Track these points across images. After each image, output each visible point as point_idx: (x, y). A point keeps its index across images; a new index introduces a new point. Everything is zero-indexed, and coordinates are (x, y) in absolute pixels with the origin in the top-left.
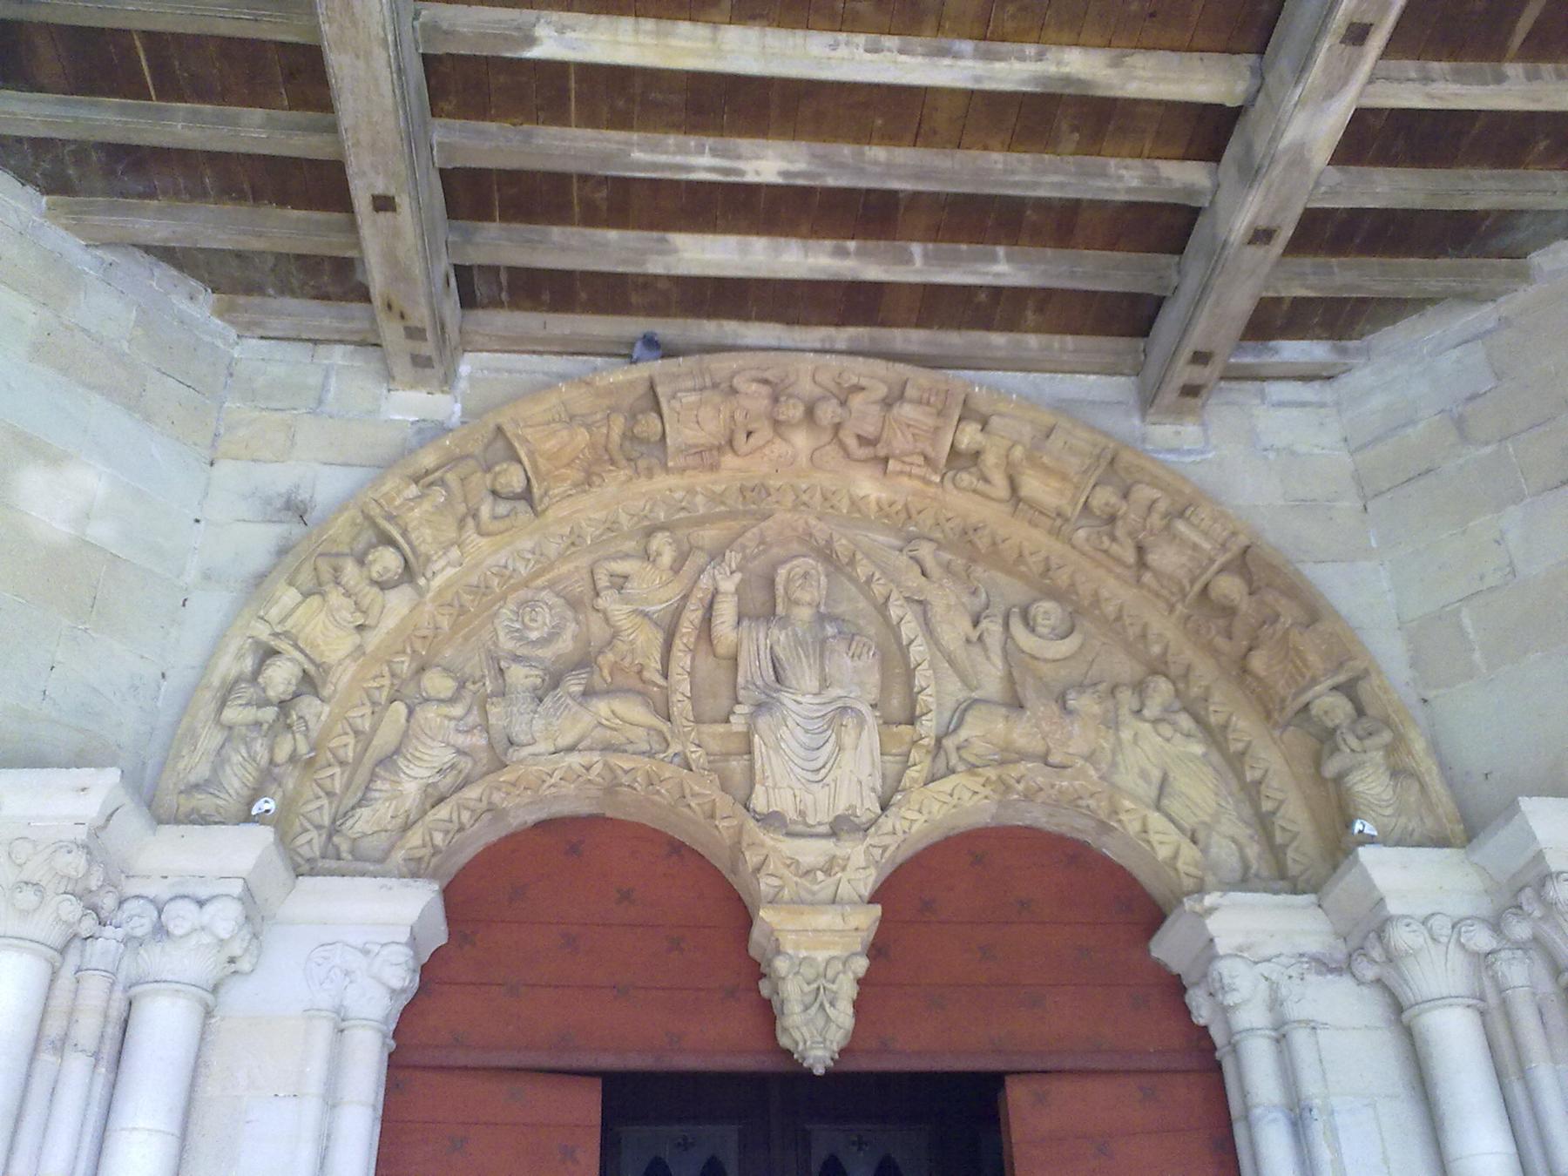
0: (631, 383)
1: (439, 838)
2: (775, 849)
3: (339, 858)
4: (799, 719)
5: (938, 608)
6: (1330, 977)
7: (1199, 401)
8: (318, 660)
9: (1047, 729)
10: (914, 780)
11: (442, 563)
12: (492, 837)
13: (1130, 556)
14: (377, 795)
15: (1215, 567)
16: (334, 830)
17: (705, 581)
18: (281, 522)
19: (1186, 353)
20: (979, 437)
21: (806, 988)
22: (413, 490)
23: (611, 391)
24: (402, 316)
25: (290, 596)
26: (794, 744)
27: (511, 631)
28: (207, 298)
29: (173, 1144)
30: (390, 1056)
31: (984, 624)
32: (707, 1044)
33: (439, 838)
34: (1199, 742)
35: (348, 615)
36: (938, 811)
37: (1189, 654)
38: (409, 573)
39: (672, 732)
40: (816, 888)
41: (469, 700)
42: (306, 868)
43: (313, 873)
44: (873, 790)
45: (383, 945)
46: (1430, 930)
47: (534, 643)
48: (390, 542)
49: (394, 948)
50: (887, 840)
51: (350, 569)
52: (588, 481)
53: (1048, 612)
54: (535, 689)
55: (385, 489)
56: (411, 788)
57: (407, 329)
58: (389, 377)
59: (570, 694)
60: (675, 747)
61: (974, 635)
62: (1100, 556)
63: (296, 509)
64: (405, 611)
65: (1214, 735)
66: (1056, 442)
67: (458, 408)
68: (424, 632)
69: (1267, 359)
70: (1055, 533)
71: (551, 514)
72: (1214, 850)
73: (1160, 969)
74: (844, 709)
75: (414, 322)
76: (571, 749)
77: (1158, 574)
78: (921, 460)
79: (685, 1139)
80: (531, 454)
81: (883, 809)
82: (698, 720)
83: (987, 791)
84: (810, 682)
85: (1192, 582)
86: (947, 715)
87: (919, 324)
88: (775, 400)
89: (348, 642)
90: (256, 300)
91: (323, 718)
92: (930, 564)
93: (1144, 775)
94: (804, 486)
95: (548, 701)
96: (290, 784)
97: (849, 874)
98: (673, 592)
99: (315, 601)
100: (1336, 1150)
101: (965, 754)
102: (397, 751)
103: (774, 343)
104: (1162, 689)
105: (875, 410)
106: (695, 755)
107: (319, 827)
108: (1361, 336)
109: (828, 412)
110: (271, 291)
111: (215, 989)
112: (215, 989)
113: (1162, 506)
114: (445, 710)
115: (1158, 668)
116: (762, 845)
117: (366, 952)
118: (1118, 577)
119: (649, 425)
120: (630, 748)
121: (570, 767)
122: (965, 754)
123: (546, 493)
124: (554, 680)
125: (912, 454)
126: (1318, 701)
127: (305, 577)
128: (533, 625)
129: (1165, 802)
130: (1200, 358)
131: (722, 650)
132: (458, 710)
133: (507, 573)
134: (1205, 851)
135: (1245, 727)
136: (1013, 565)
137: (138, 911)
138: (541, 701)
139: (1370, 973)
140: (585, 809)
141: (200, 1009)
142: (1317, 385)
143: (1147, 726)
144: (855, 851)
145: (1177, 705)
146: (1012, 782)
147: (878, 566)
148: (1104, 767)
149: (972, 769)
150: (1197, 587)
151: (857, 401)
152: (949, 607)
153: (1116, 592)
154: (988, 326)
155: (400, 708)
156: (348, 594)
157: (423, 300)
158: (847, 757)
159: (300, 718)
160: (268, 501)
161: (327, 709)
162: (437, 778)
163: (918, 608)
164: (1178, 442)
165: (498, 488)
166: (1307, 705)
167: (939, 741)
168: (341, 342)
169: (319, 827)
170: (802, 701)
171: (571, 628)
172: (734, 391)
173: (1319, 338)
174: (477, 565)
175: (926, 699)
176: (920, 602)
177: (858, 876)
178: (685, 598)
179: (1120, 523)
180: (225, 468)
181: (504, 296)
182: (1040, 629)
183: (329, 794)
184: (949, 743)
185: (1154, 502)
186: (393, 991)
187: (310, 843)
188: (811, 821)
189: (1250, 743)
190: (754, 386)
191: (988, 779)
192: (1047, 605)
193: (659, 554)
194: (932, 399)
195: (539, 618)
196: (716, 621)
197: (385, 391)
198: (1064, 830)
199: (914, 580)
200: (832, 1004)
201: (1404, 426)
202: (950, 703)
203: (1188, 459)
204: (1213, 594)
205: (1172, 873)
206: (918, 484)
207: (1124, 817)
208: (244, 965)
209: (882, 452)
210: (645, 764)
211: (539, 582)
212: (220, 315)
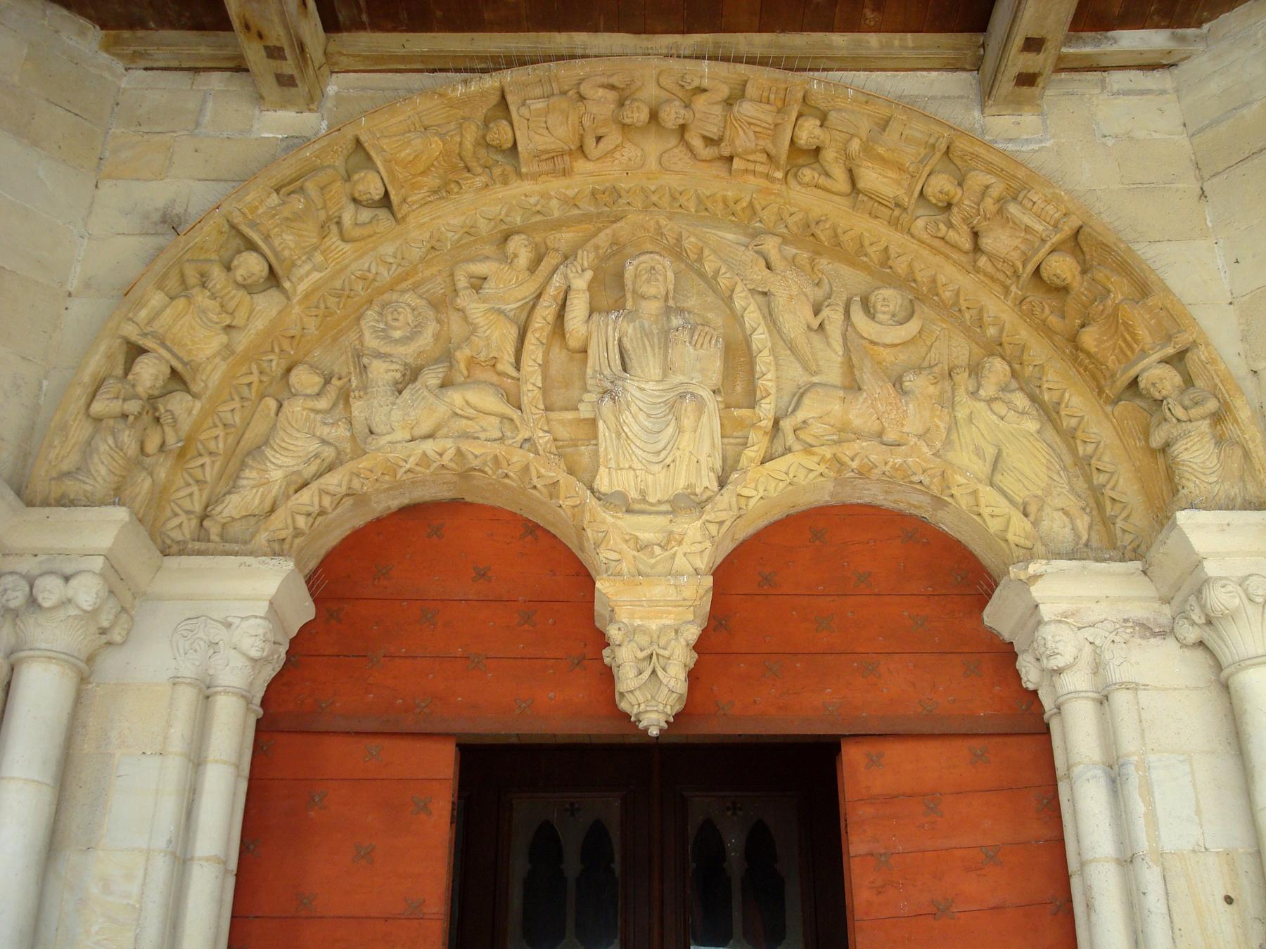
0: (483, 94)
1: (301, 522)
2: (614, 525)
4: (641, 404)
6: (1152, 640)
7: (1035, 91)
8: (186, 359)
10: (752, 460)
11: (307, 267)
12: (359, 522)
13: (967, 245)
15: (1047, 246)
17: (557, 280)
19: (1018, 41)
20: (818, 131)
21: (641, 655)
23: (465, 101)
24: (260, 36)
25: (157, 299)
26: (636, 428)
27: (375, 331)
28: (95, 34)
29: (47, 795)
30: (258, 721)
31: (825, 312)
32: (541, 708)
33: (301, 522)
36: (774, 490)
37: (1024, 334)
38: (273, 279)
40: (653, 561)
41: (334, 395)
42: (175, 548)
43: (181, 553)
44: (712, 469)
46: (1246, 591)
47: (396, 341)
48: (252, 246)
49: (253, 621)
50: (722, 516)
51: (217, 273)
52: (443, 191)
53: (889, 299)
54: (396, 383)
55: (249, 198)
56: (277, 475)
57: (266, 48)
61: (815, 324)
62: (937, 243)
64: (274, 313)
65: (1049, 413)
66: (891, 136)
67: (324, 124)
68: (292, 333)
69: (1107, 47)
70: (894, 223)
71: (411, 219)
72: (1045, 524)
73: (993, 636)
74: (682, 396)
75: (272, 42)
76: (430, 436)
77: (991, 257)
78: (763, 158)
79: (572, 804)
80: (387, 162)
81: (722, 484)
83: (822, 468)
84: (654, 370)
86: (786, 399)
87: (760, 30)
88: (621, 104)
89: (218, 341)
90: (141, 33)
91: (195, 412)
92: (774, 256)
94: (653, 188)
95: (406, 393)
96: (162, 474)
97: (685, 548)
98: (529, 289)
99: (181, 303)
100: (1150, 803)
101: (802, 435)
105: (718, 110)
106: (543, 439)
107: (188, 512)
108: (1199, 25)
109: (672, 114)
111: (90, 660)
112: (90, 660)
113: (995, 192)
114: (310, 404)
115: (995, 348)
116: (604, 522)
118: (955, 263)
119: (500, 133)
120: (483, 436)
121: (424, 454)
122: (802, 435)
123: (405, 200)
124: (412, 375)
125: (754, 152)
126: (1145, 374)
127: (173, 283)
128: (396, 324)
129: (998, 478)
130: (1033, 45)
131: (573, 343)
132: (323, 404)
133: (371, 276)
134: (1035, 524)
135: (1079, 405)
136: (852, 255)
138: (400, 393)
139: (1192, 635)
140: (445, 493)
143: (982, 404)
145: (1014, 385)
146: (847, 459)
147: (725, 261)
148: (938, 445)
149: (808, 449)
150: (1031, 267)
151: (700, 102)
152: (791, 297)
153: (953, 277)
154: (830, 28)
156: (213, 297)
157: (276, 20)
158: (686, 440)
161: (198, 405)
163: (759, 298)
164: (1017, 131)
165: (357, 195)
167: (776, 422)
169: (188, 512)
170: (644, 389)
171: (431, 328)
172: (582, 98)
173: (1157, 26)
174: (342, 270)
175: (767, 382)
176: (765, 294)
179: (955, 210)
181: (364, 17)
182: (880, 316)
185: (987, 187)
186: (254, 660)
187: (181, 527)
188: (652, 500)
190: (601, 92)
191: (823, 458)
192: (888, 293)
193: (516, 256)
194: (772, 97)
195: (401, 318)
196: (569, 316)
199: (758, 273)
204: (1045, 275)
205: (1003, 544)
206: (764, 183)
207: (954, 491)
208: (117, 637)
209: (726, 152)
210: (496, 448)
211: (404, 285)
212: (107, 51)
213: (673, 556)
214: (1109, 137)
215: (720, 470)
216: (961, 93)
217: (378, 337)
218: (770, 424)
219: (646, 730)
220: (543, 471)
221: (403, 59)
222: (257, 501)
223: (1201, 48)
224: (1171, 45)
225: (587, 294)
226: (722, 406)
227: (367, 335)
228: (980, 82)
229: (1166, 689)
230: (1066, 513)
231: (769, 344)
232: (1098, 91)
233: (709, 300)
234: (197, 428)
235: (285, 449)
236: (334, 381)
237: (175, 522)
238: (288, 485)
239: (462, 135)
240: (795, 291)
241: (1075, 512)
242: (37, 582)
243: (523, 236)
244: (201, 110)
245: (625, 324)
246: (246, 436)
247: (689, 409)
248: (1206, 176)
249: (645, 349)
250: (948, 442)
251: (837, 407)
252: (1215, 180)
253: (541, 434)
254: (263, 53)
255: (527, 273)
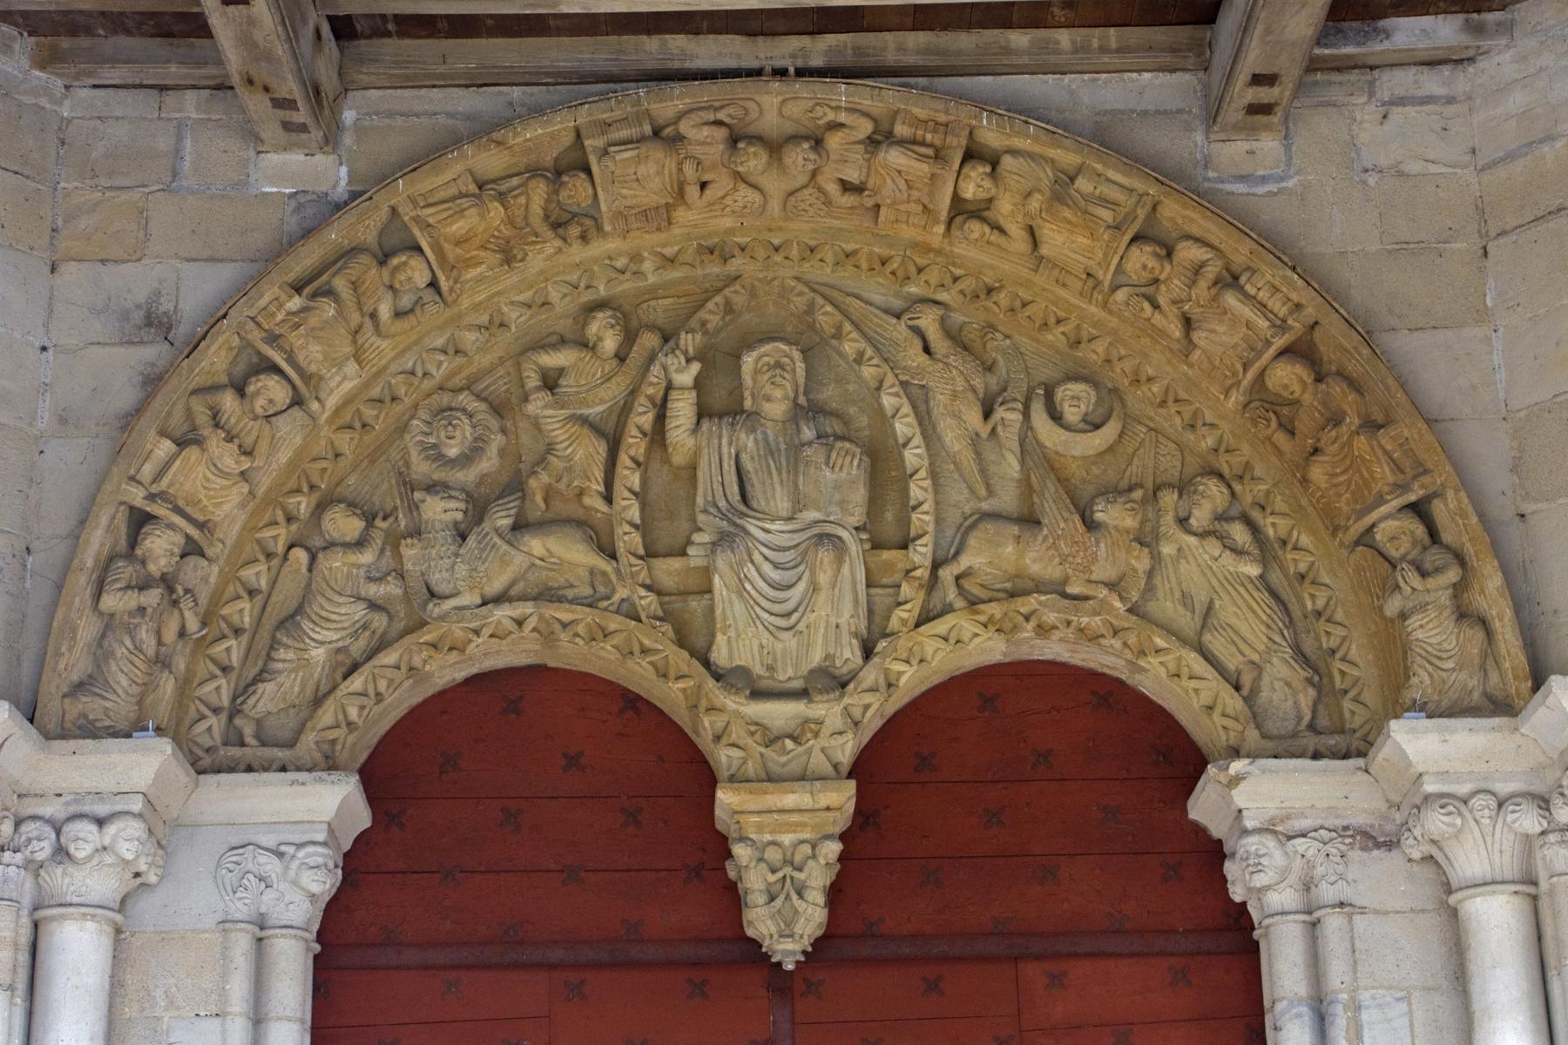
3: (242, 744)
5: (940, 399)
6: (1376, 853)
8: (201, 518)
9: (1066, 551)
10: (904, 622)
14: (280, 666)
15: (1272, 351)
16: (235, 711)
18: (141, 342)
19: (1242, 77)
20: (987, 183)
21: (772, 878)
22: (296, 303)
24: (266, 89)
26: (761, 584)
27: (425, 448)
31: (999, 413)
34: (1255, 560)
35: (230, 460)
39: (618, 572)
40: (784, 759)
41: (379, 542)
45: (300, 846)
47: (452, 463)
56: (318, 654)
57: (272, 100)
58: (254, 138)
59: (496, 530)
60: (621, 593)
63: (156, 323)
64: (298, 440)
73: (1199, 830)
76: (500, 599)
81: (868, 652)
82: (650, 553)
85: (1245, 367)
86: (949, 533)
91: (212, 580)
93: (1186, 600)
95: (472, 541)
97: (823, 741)
98: (615, 390)
99: (193, 453)
101: (966, 583)
102: (299, 610)
103: (731, 63)
104: (1213, 495)
105: (858, 154)
107: (216, 711)
110: (101, 32)
117: (280, 855)
122: (966, 583)
124: (478, 509)
126: (1382, 525)
131: (678, 459)
132: (367, 557)
135: (1308, 548)
137: (35, 833)
141: (110, 930)
142: (1446, 70)
144: (827, 710)
150: (1251, 375)
152: (954, 395)
155: (300, 555)
159: (187, 591)
160: (125, 316)
162: (348, 641)
164: (1247, 159)
166: (1370, 529)
168: (194, 87)
171: (498, 440)
172: (679, 138)
177: (833, 743)
178: (633, 393)
180: (69, 270)
183: (225, 669)
184: (947, 574)
185: (1203, 264)
189: (1313, 563)
190: (706, 131)
193: (600, 339)
195: (458, 433)
196: (671, 424)
197: (252, 153)
198: (1092, 665)
199: (913, 356)
200: (800, 895)
201: (1541, 142)
202: (953, 517)
203: (1261, 190)
213: (809, 752)
214: (1374, 165)
215: (864, 632)
216: (1182, 105)
217: (427, 458)
218: (927, 574)
219: (779, 964)
220: (647, 642)
221: (442, 76)
222: (296, 689)
223: (1504, 42)
224: (1463, 39)
225: (694, 394)
226: (867, 546)
227: (415, 456)
228: (1207, 87)
229: (1387, 913)
230: (1288, 685)
231: (926, 463)
232: (1364, 99)
233: (851, 388)
234: (217, 600)
235: (328, 620)
236: (379, 523)
237: (203, 726)
238: (334, 669)
239: (528, 198)
240: (960, 384)
241: (1297, 684)
242: (65, 829)
243: (609, 313)
244: (177, 151)
245: (743, 436)
246: (273, 599)
247: (826, 560)
248: (1493, 234)
249: (770, 473)
250: (1150, 589)
251: (1010, 549)
252: (1502, 241)
253: (643, 592)
254: (269, 103)
255: (615, 362)
